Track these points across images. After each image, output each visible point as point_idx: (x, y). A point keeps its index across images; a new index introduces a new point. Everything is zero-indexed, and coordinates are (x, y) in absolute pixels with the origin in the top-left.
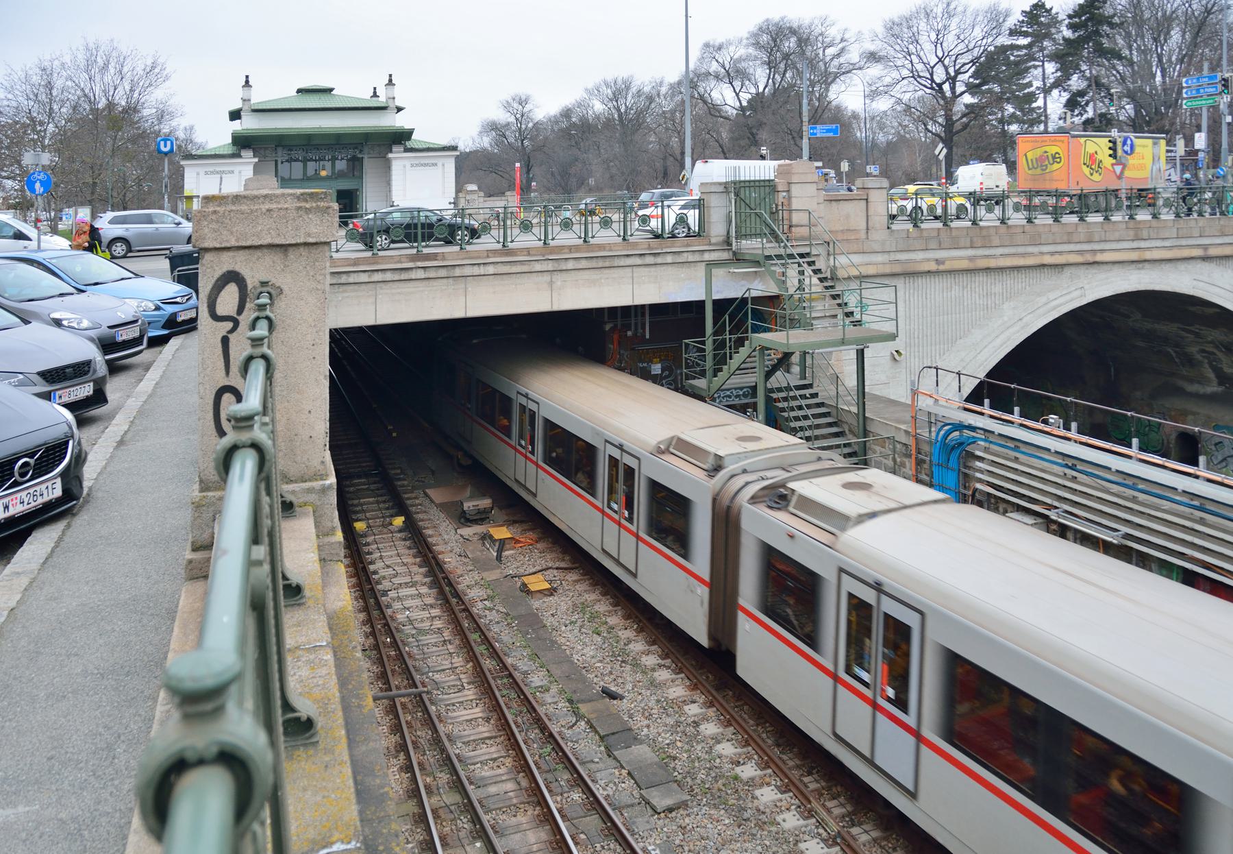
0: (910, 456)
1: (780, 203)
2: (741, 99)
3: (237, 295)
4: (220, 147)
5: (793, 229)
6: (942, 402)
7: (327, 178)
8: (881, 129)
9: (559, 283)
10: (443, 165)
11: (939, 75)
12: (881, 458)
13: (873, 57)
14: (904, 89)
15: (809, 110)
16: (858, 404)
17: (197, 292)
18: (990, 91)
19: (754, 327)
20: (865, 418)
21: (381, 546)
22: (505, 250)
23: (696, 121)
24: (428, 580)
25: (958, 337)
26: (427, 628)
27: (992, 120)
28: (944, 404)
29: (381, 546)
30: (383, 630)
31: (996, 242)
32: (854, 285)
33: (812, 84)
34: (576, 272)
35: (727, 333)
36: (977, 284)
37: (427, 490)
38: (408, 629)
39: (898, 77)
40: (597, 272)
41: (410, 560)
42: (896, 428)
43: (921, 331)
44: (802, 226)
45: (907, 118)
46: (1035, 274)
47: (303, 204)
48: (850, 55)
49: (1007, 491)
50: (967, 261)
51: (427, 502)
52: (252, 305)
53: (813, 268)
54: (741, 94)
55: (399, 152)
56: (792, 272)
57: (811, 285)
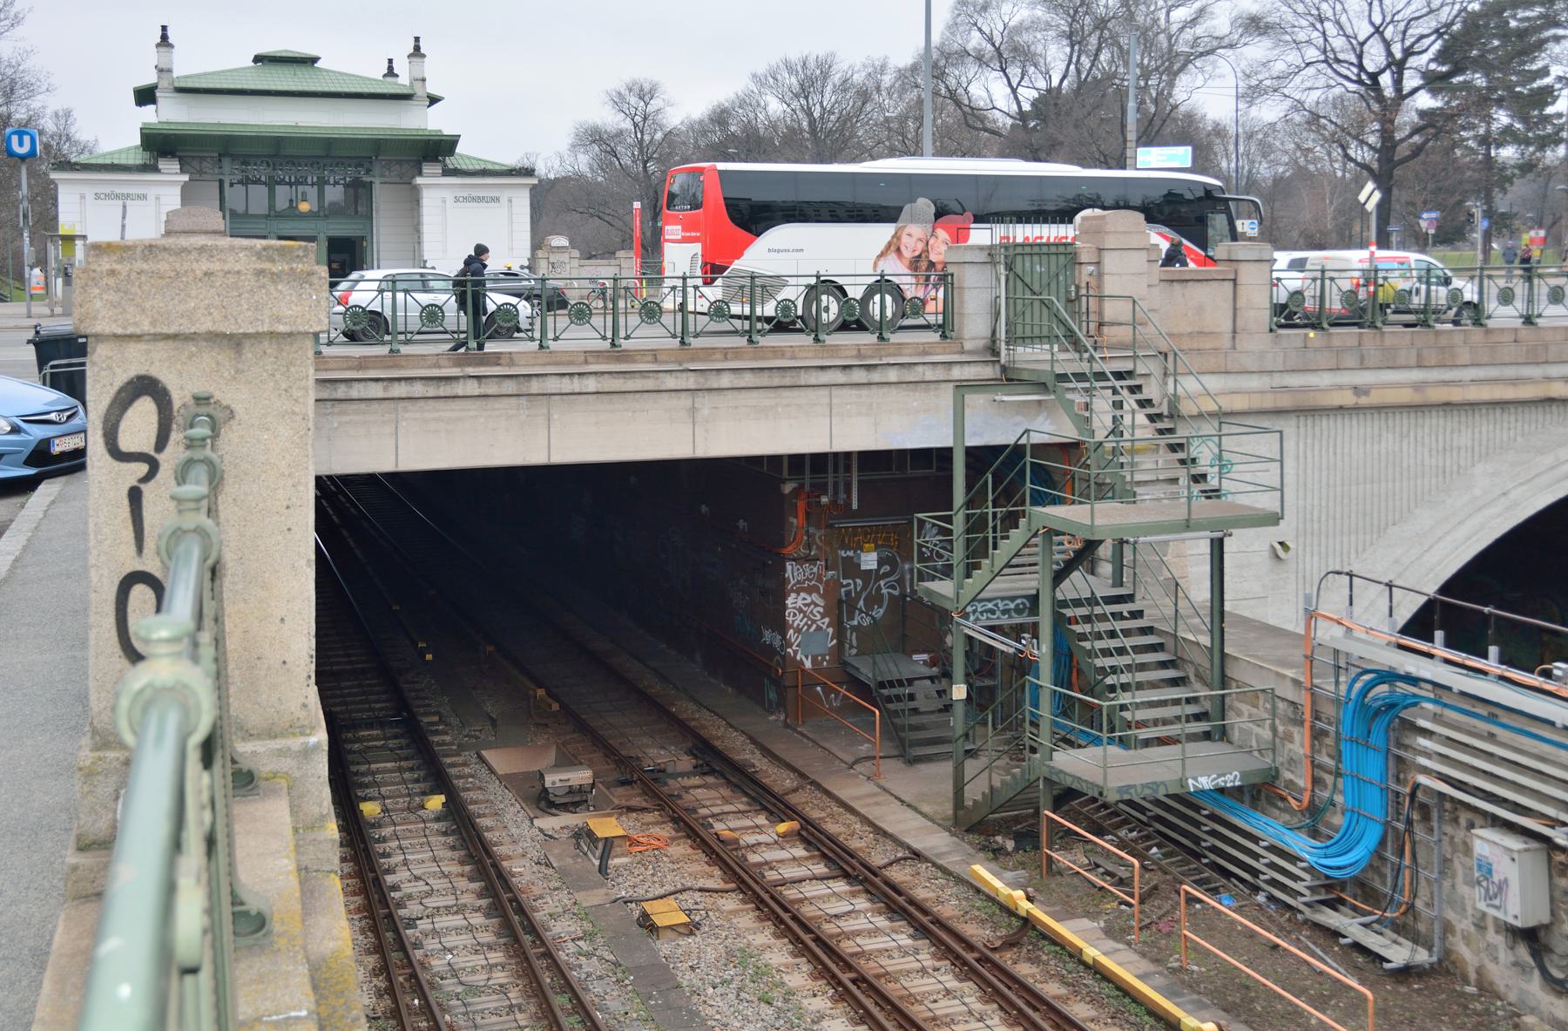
0: (1301, 723)
1: (1083, 285)
2: (1021, 98)
3: (153, 419)
4: (120, 152)
5: (1106, 329)
6: (1359, 633)
7: (310, 215)
8: (1265, 156)
9: (706, 412)
10: (510, 201)
11: (1374, 58)
12: (1251, 725)
13: (1255, 25)
14: (1308, 84)
15: (1138, 120)
16: (1211, 631)
17: (84, 404)
18: (1466, 86)
19: (1036, 495)
20: (1223, 655)
21: (405, 843)
22: (615, 352)
23: (942, 137)
24: (484, 902)
25: (1390, 524)
26: (482, 983)
27: (1468, 139)
28: (1363, 636)
29: (405, 843)
30: (407, 985)
31: (1464, 356)
32: (1209, 428)
33: (1146, 74)
34: (735, 393)
35: (990, 504)
36: (1427, 430)
37: (484, 753)
38: (449, 985)
39: (1299, 61)
40: (771, 393)
41: (455, 868)
42: (1278, 674)
43: (1324, 510)
44: (1121, 324)
45: (1312, 136)
46: (1537, 415)
47: (267, 265)
48: (1215, 22)
49: (1473, 791)
50: (1410, 390)
51: (484, 771)
52: (181, 436)
53: (1139, 396)
54: (1020, 90)
55: (434, 175)
56: (1102, 405)
57: (1133, 426)
